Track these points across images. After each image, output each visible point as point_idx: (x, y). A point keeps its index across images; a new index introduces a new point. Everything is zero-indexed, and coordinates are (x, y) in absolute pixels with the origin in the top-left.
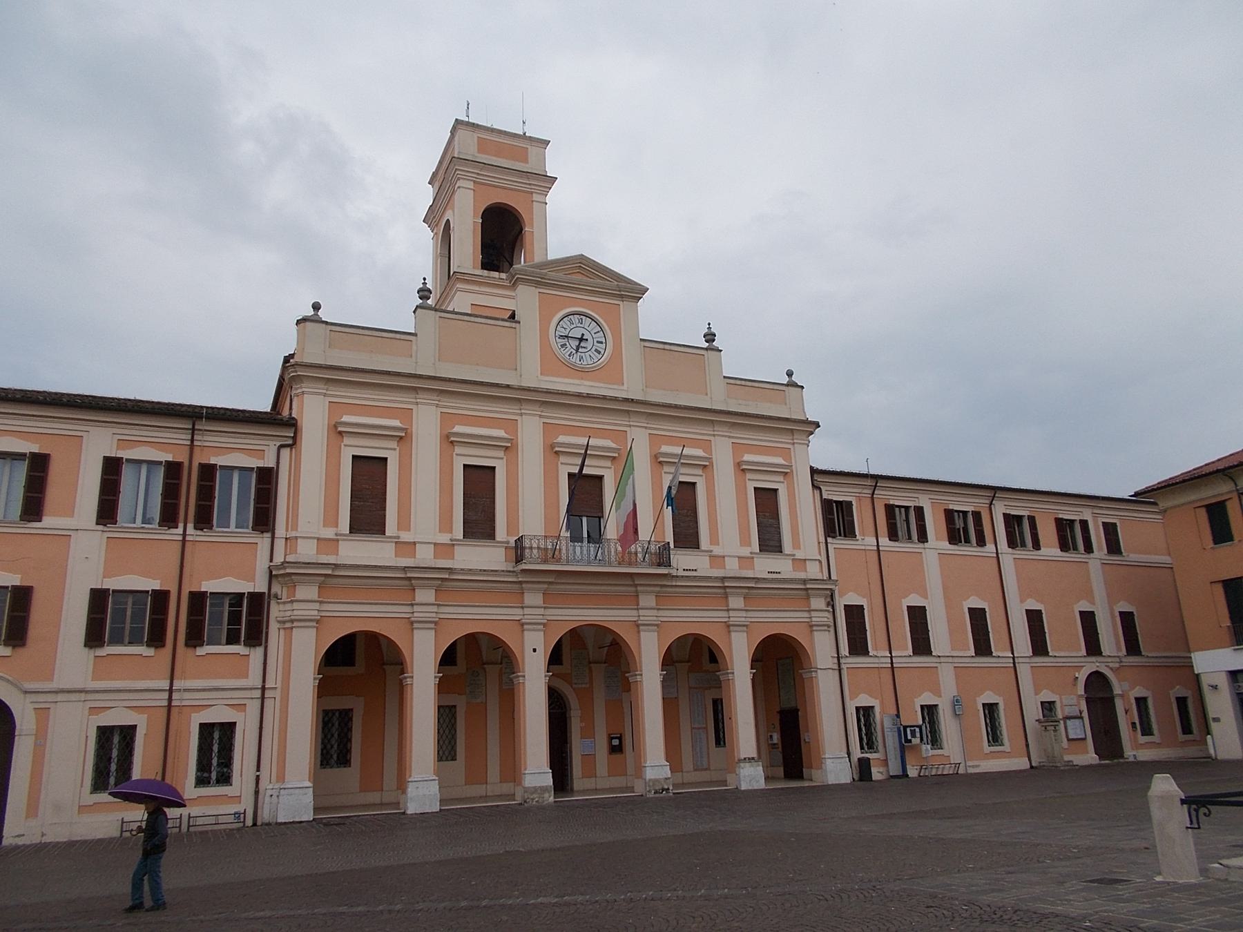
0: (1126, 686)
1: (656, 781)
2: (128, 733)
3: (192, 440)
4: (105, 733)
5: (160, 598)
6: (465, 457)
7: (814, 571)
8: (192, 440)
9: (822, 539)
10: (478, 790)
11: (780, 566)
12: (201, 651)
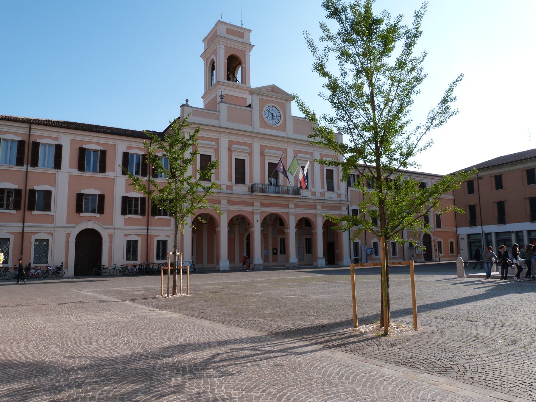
0: (435, 238)
1: (293, 263)
2: (165, 243)
4: (129, 242)
5: (18, 192)
6: (326, 167)
12: (82, 215)
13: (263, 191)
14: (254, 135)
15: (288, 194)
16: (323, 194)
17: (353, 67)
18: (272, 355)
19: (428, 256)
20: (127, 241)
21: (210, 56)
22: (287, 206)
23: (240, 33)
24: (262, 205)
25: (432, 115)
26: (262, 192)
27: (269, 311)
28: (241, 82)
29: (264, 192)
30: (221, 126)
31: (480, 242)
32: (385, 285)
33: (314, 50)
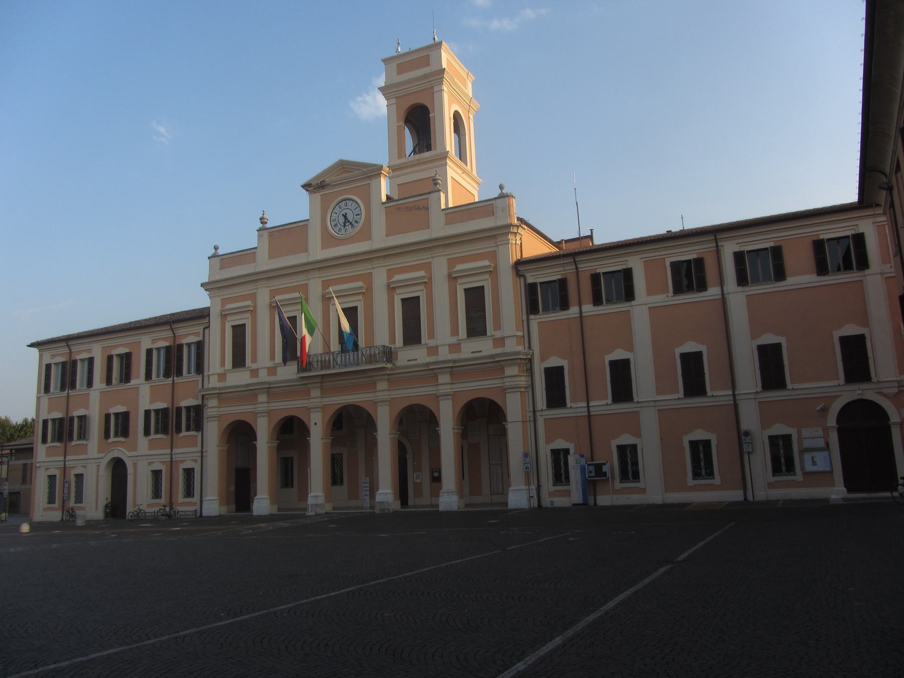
3: (577, 268)
7: (511, 346)
8: (577, 268)
9: (525, 317)
11: (484, 347)
15: (358, 364)
16: (455, 347)
20: (770, 437)
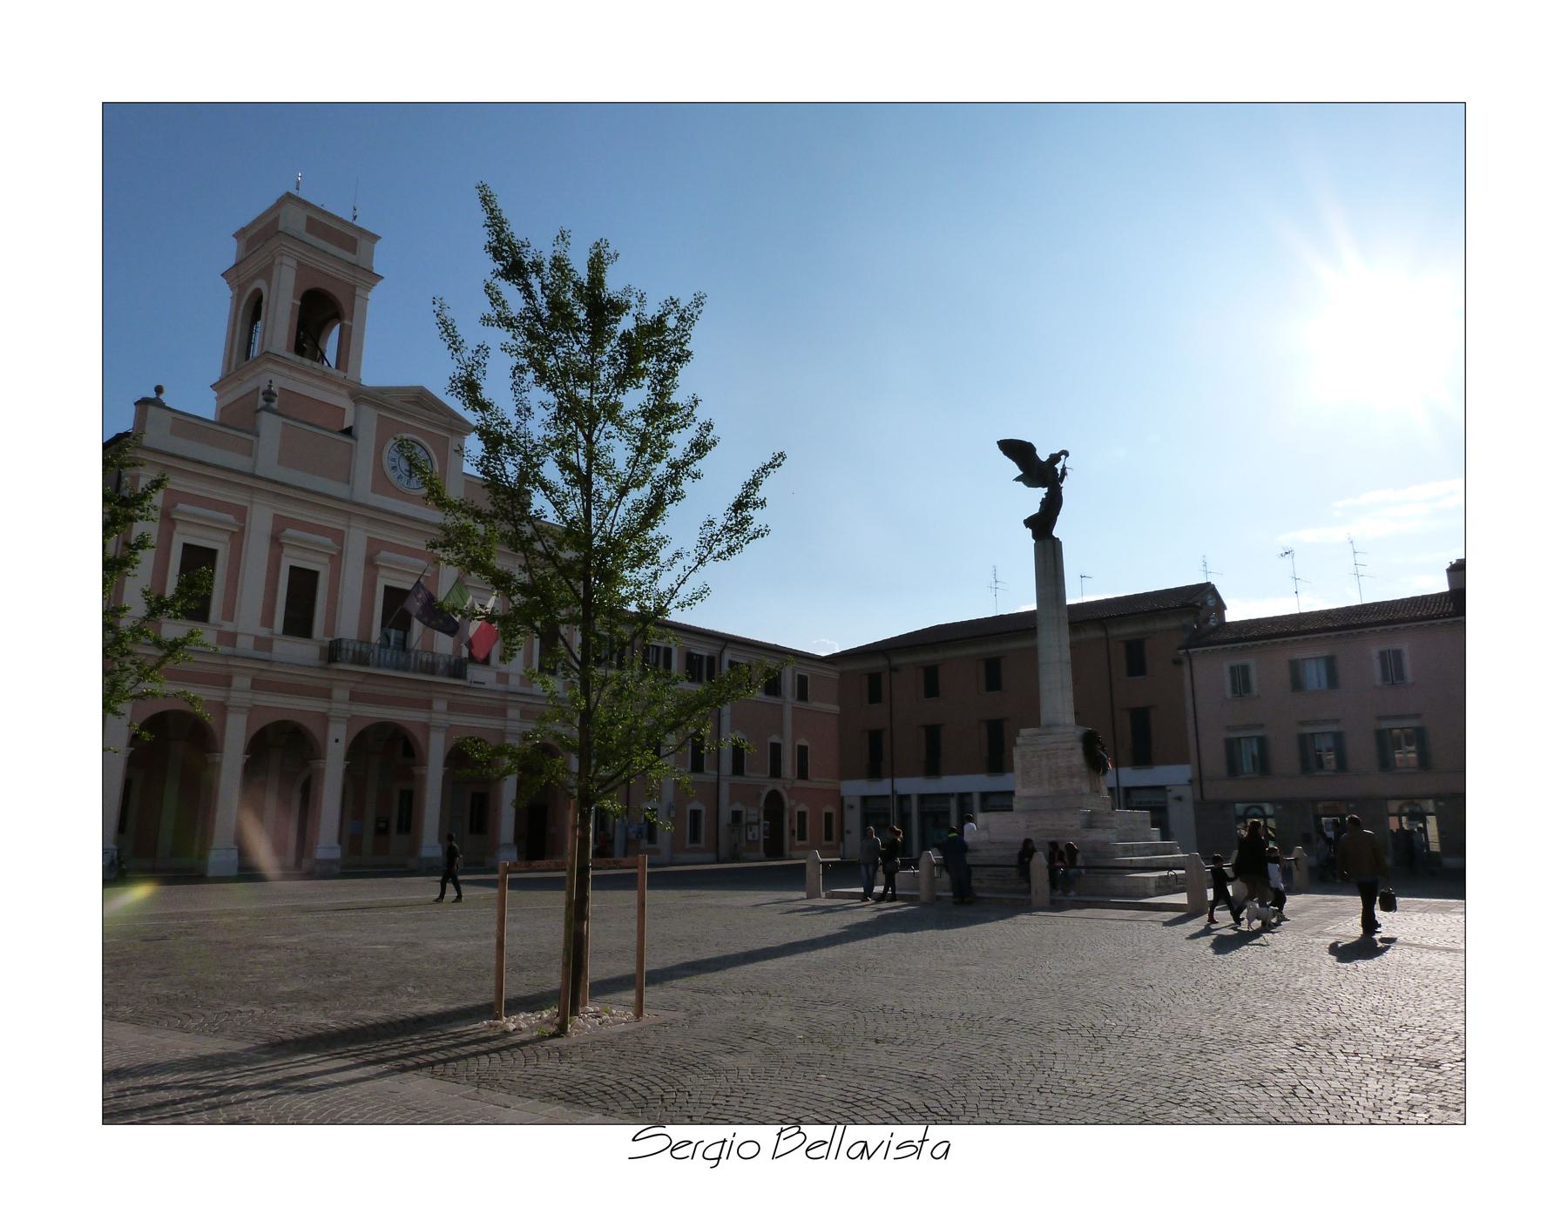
0: (793, 802)
10: (1238, 661)
13: (361, 659)
14: (355, 510)
17: (551, 398)
18: (232, 1098)
19: (774, 847)
21: (254, 278)
22: (427, 705)
23: (349, 238)
24: (355, 697)
25: (708, 532)
26: (360, 663)
27: (295, 986)
28: (333, 364)
29: (366, 663)
30: (258, 473)
31: (887, 815)
32: (577, 912)
33: (455, 344)
